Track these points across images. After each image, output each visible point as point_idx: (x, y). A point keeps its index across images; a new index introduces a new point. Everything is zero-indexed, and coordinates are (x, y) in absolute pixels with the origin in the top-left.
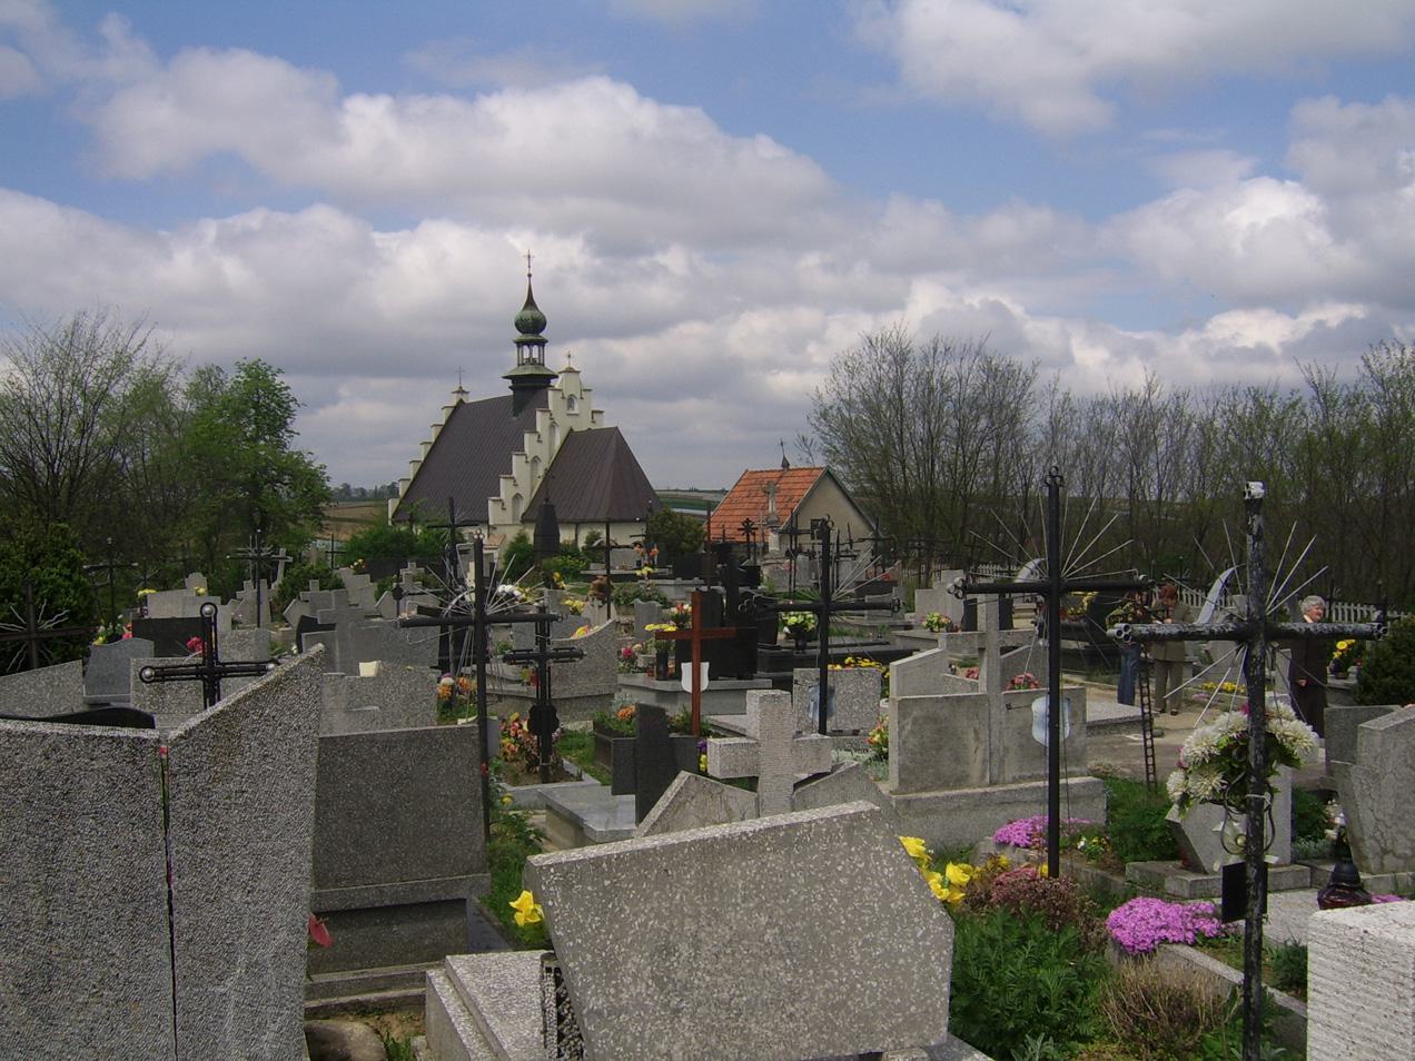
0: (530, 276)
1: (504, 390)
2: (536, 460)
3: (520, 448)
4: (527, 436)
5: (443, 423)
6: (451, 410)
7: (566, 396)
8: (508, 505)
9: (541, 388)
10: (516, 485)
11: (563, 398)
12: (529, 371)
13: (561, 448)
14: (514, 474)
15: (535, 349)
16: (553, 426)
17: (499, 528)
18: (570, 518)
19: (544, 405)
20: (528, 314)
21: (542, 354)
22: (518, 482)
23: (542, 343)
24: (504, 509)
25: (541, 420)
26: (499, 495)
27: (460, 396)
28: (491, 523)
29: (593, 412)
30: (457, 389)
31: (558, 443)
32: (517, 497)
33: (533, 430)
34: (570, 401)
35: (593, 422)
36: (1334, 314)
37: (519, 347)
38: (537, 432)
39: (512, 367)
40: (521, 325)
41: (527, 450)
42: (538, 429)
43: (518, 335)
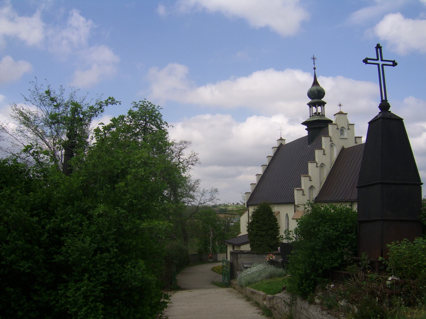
0: (315, 69)
1: (303, 132)
2: (322, 165)
3: (313, 160)
4: (310, 165)
5: (272, 155)
6: (276, 149)
7: (339, 127)
8: (307, 192)
9: (323, 128)
10: (310, 180)
11: (338, 129)
12: (316, 118)
13: (338, 158)
14: (310, 174)
15: (319, 108)
16: (332, 146)
17: (257, 312)
18: (347, 198)
19: (327, 135)
20: (315, 88)
21: (323, 110)
22: (312, 179)
23: (323, 104)
24: (304, 195)
25: (325, 141)
26: (301, 187)
27: (281, 142)
28: (296, 203)
29: (356, 137)
30: (279, 138)
31: (335, 155)
32: (312, 187)
33: (320, 148)
34: (342, 130)
35: (356, 143)
36: (251, 210)
37: (310, 107)
38: (322, 149)
39: (306, 117)
40: (311, 94)
41: (317, 160)
42: (323, 147)
43: (309, 100)
